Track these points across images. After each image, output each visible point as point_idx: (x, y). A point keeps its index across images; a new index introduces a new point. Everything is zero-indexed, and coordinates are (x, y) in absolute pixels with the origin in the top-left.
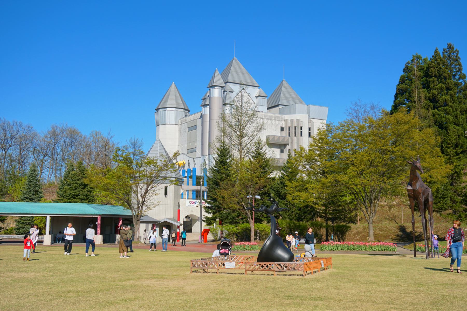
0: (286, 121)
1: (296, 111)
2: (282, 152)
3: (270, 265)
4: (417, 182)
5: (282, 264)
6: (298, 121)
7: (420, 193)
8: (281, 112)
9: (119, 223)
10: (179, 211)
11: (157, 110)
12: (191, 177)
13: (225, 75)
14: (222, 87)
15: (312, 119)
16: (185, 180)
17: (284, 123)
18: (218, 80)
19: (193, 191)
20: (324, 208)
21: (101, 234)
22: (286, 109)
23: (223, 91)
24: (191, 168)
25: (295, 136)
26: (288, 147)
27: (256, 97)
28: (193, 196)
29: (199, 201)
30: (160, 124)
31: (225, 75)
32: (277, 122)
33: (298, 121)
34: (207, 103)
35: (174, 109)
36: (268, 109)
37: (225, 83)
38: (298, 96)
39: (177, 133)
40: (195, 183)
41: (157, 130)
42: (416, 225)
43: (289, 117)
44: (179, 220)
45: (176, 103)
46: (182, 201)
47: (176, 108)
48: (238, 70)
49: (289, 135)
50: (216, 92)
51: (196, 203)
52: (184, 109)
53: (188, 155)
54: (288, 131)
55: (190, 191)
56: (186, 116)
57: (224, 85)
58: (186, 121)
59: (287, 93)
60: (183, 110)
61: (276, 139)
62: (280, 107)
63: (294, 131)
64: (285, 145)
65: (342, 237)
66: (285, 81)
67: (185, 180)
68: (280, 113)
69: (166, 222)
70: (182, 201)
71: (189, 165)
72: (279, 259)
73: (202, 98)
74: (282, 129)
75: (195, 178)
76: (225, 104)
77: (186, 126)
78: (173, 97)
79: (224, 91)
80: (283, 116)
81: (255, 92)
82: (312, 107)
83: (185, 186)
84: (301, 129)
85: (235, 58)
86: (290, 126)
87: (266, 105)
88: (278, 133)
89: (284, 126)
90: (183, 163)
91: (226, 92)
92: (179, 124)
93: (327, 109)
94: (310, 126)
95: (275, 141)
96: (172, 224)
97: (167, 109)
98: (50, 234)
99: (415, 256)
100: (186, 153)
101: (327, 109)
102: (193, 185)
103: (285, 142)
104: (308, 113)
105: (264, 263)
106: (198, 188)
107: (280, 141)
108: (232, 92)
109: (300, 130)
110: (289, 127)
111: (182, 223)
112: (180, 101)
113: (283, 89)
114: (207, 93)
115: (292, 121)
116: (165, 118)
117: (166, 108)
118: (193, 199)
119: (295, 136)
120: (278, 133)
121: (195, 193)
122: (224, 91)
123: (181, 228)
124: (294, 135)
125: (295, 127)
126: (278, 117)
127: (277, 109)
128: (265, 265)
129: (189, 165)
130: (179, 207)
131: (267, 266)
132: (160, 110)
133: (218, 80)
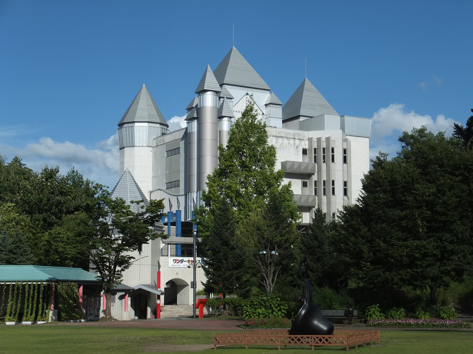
0: (310, 140)
1: (324, 125)
2: (305, 185)
3: (330, 338)
6: (328, 139)
8: (303, 127)
10: (159, 273)
11: (121, 125)
12: (173, 224)
13: (220, 75)
15: (347, 137)
17: (307, 142)
18: (211, 81)
19: (177, 244)
22: (314, 122)
23: (218, 98)
25: (324, 162)
26: (315, 178)
27: (266, 105)
29: (192, 259)
30: (125, 145)
31: (220, 75)
32: (297, 142)
33: (328, 139)
34: (195, 116)
35: (146, 124)
36: (284, 121)
37: (221, 86)
42: (291, 140)
43: (315, 134)
44: (159, 286)
46: (162, 260)
48: (238, 64)
50: (209, 100)
51: (182, 261)
52: (161, 124)
53: (167, 191)
55: (173, 244)
56: (163, 134)
57: (219, 89)
59: (312, 100)
60: (158, 125)
61: (296, 166)
62: (302, 119)
63: (322, 154)
64: (309, 176)
65: (47, 306)
69: (140, 290)
70: (162, 260)
71: (171, 206)
73: (187, 106)
74: (305, 152)
75: (179, 225)
76: (221, 117)
77: (164, 148)
78: (144, 105)
79: (220, 98)
81: (265, 97)
82: (348, 120)
85: (234, 48)
86: (316, 147)
87: (281, 116)
88: (299, 158)
91: (222, 99)
94: (345, 148)
95: (295, 169)
97: (136, 124)
100: (164, 188)
102: (177, 236)
103: (309, 171)
104: (343, 127)
105: (318, 336)
106: (189, 240)
107: (302, 170)
108: (231, 99)
109: (331, 154)
111: (163, 290)
112: (155, 112)
113: (305, 93)
114: (193, 101)
115: (319, 140)
117: (134, 122)
118: (177, 256)
119: (324, 162)
120: (299, 158)
121: (179, 246)
122: (220, 98)
123: (162, 297)
124: (322, 160)
125: (324, 149)
127: (296, 121)
128: (324, 338)
129: (171, 206)
130: (159, 267)
131: (327, 340)
132: (125, 125)
133: (211, 81)
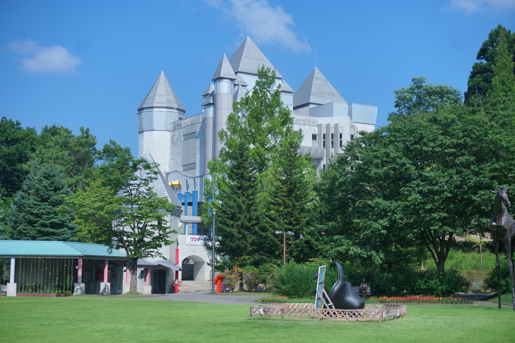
0: (319, 126)
4: (502, 216)
5: (354, 311)
6: (336, 126)
7: (506, 230)
8: (312, 113)
9: (109, 268)
10: (177, 250)
11: (140, 110)
12: (190, 204)
14: (232, 80)
15: (355, 124)
16: (183, 208)
17: (316, 128)
18: (227, 70)
19: (193, 223)
20: (99, 227)
21: (82, 282)
23: (233, 85)
24: (191, 191)
28: (193, 231)
33: (336, 126)
35: (165, 110)
37: (236, 73)
38: (335, 91)
39: (168, 143)
40: (196, 212)
41: (140, 139)
43: (323, 121)
44: (177, 263)
45: (167, 100)
47: (167, 108)
49: (324, 146)
50: (225, 87)
52: (178, 109)
53: (184, 173)
54: (322, 140)
57: (233, 76)
58: (181, 125)
62: (311, 106)
63: (331, 140)
66: (317, 70)
67: (183, 208)
68: (310, 115)
69: (159, 265)
72: (349, 306)
75: (195, 205)
77: (182, 132)
79: (235, 85)
80: (316, 119)
83: (183, 217)
84: (341, 137)
86: (325, 133)
89: (316, 133)
90: (179, 185)
92: (171, 130)
93: (376, 109)
94: (353, 134)
96: (168, 268)
97: (155, 110)
98: (15, 282)
99: (500, 307)
101: (376, 109)
102: (193, 215)
103: (318, 155)
104: (350, 114)
108: (245, 86)
109: (339, 139)
110: (324, 135)
112: (172, 98)
113: (315, 82)
116: (152, 122)
117: (153, 107)
119: (333, 147)
121: (196, 225)
124: (331, 145)
125: (332, 135)
126: (309, 121)
127: (306, 109)
129: (188, 188)
133: (227, 70)
